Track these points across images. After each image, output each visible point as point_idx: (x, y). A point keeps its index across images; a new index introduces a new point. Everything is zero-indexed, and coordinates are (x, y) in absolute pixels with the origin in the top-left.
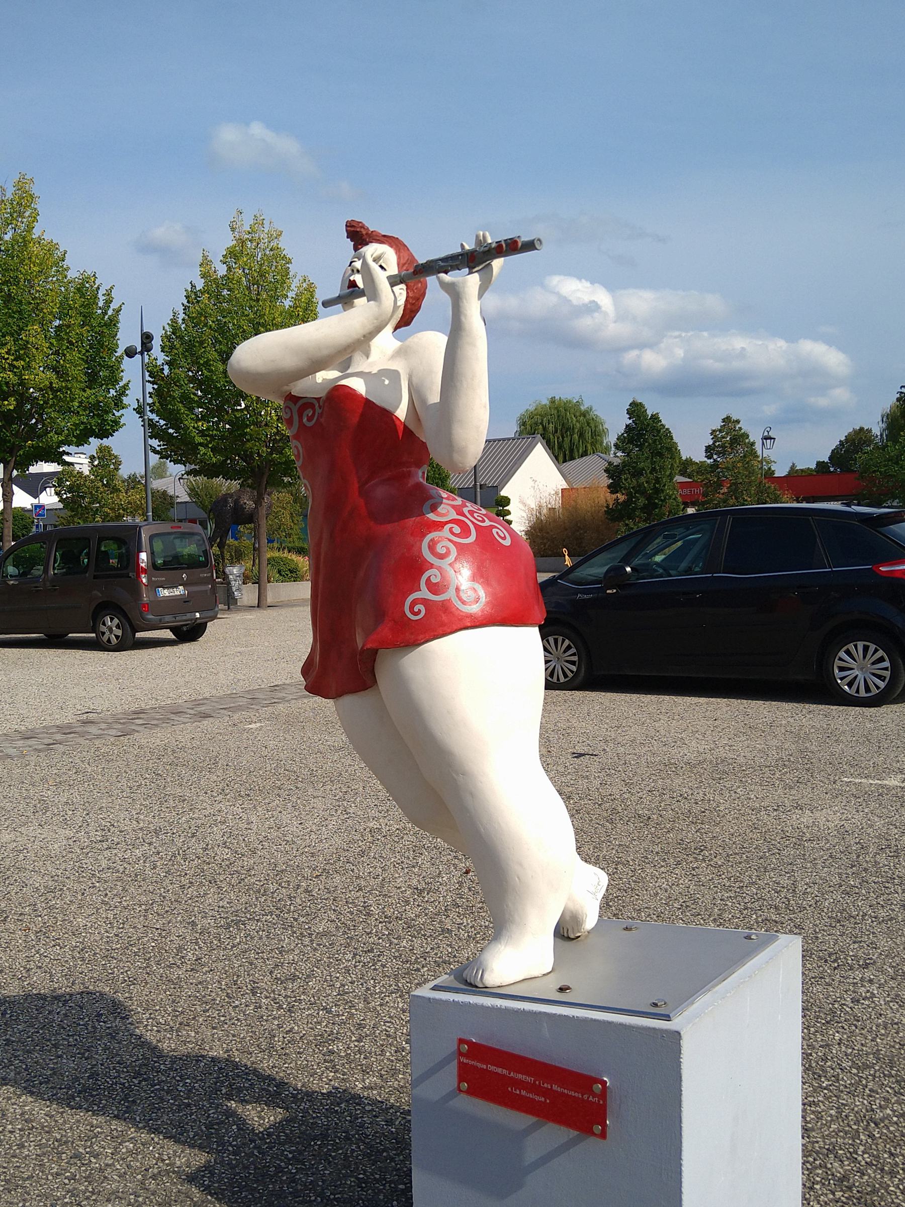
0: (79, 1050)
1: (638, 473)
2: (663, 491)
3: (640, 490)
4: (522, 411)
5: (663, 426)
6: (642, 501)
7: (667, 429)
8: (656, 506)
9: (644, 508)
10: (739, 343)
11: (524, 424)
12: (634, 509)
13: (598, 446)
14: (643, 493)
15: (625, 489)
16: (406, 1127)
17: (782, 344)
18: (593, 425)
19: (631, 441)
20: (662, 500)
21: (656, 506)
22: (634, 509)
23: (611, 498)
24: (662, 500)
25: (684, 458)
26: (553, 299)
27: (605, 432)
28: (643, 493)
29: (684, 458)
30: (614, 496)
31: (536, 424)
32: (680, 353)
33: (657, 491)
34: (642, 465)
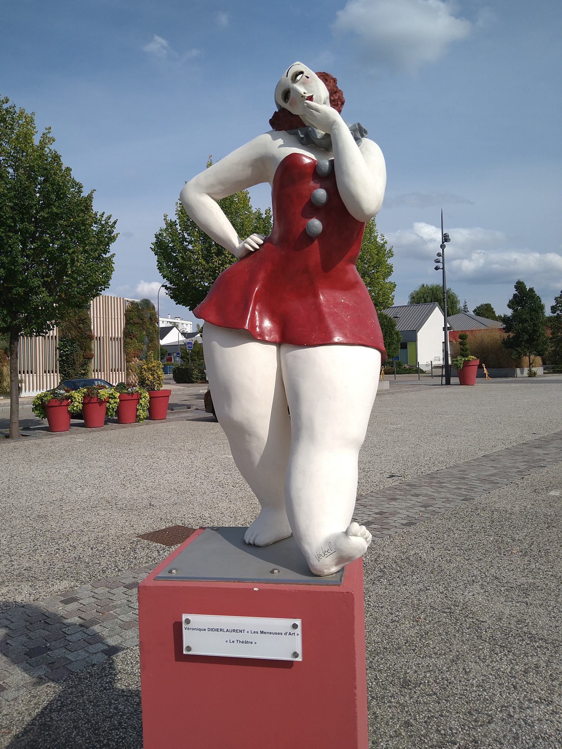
0: (38, 639)
1: (523, 321)
2: (538, 331)
3: (524, 330)
4: (412, 291)
5: (536, 295)
6: (526, 337)
7: (538, 296)
8: (534, 340)
9: (527, 341)
10: (515, 256)
11: (413, 298)
12: (521, 341)
13: (454, 309)
14: (527, 332)
15: (516, 330)
16: (137, 712)
17: (537, 255)
18: (451, 298)
19: (518, 304)
20: (538, 336)
21: (534, 340)
22: (521, 341)
23: (505, 335)
24: (538, 336)
25: (497, 315)
26: (413, 238)
27: (458, 302)
28: (527, 332)
29: (497, 315)
30: (508, 334)
31: (420, 298)
32: (482, 261)
33: (535, 331)
34: (524, 316)
